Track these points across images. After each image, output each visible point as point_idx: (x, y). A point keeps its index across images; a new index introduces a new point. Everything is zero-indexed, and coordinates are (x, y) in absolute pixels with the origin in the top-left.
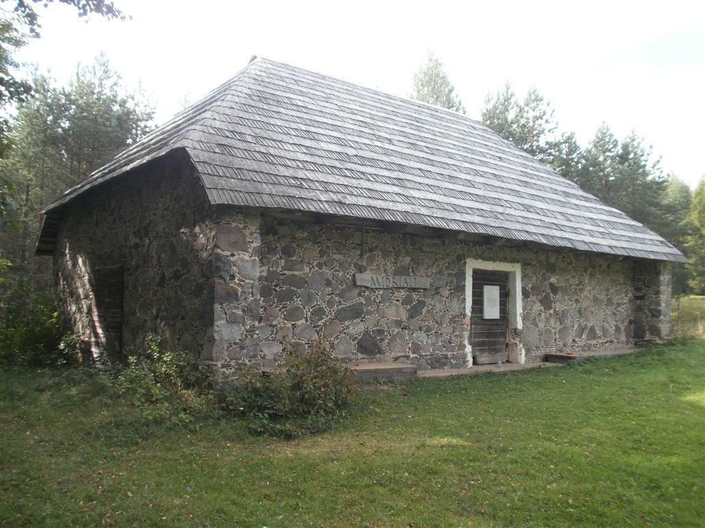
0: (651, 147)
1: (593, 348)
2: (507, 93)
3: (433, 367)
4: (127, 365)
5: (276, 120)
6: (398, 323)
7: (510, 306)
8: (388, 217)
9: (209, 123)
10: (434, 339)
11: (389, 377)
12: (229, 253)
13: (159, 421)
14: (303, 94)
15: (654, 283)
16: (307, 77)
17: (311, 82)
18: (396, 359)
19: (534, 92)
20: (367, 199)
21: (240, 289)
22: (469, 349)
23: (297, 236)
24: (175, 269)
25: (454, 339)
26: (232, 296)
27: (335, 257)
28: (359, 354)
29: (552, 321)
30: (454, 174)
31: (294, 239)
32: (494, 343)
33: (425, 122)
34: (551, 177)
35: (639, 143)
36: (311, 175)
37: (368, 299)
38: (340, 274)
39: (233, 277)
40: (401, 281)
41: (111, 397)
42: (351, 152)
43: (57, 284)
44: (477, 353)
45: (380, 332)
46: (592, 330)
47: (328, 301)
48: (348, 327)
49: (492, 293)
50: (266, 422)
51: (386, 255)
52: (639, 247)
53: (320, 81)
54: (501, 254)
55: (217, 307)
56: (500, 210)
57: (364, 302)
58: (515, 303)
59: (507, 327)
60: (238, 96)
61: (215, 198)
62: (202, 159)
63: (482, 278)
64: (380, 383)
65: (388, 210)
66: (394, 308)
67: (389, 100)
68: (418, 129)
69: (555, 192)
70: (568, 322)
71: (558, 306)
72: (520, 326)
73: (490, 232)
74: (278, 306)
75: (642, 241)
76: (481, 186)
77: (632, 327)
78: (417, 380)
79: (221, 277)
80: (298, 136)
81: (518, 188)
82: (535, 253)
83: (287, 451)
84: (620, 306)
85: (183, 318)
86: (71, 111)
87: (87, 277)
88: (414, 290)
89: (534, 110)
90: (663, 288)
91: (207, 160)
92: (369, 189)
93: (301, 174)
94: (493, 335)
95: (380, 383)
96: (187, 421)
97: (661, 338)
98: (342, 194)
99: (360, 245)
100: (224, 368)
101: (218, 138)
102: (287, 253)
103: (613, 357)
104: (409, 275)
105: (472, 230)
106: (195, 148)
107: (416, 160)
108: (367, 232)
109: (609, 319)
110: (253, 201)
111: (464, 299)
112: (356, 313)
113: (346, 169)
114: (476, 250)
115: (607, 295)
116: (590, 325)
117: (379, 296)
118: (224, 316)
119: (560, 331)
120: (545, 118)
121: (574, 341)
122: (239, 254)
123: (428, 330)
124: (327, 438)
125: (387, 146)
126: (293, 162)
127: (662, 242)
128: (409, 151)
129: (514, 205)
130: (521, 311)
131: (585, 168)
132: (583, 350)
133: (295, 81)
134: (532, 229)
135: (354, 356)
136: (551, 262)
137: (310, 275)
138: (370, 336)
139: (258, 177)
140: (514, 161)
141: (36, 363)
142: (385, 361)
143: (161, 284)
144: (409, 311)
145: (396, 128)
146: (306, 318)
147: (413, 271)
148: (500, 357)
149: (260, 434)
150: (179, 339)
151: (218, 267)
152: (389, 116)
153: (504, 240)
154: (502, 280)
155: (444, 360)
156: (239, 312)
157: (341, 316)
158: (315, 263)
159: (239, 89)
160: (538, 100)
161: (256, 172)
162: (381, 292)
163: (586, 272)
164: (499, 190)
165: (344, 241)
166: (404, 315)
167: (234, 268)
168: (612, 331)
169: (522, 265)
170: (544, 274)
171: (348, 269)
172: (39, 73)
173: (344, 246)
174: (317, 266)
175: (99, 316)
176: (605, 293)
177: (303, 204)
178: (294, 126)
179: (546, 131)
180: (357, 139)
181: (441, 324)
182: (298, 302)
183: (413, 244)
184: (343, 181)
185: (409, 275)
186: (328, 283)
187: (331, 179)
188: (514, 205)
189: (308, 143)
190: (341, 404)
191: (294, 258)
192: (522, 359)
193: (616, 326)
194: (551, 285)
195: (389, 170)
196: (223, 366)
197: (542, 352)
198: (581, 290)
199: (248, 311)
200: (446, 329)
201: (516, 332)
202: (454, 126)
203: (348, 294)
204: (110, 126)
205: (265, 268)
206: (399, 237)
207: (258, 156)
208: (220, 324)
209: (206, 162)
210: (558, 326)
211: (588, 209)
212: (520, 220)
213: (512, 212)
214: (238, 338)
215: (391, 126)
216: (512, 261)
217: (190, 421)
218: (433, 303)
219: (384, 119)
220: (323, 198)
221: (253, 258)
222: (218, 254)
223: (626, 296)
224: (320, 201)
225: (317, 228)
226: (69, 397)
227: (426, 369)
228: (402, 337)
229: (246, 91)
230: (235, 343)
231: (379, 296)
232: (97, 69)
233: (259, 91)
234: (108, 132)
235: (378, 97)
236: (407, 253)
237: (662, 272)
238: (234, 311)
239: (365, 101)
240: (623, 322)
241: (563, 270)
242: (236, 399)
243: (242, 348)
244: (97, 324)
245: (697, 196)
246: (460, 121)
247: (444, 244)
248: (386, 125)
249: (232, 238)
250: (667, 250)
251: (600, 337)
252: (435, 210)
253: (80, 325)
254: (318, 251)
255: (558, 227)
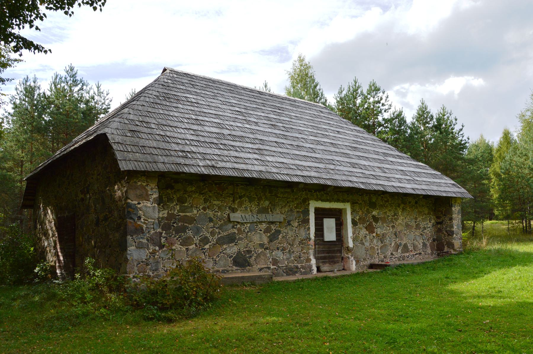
0: (456, 120)
1: (406, 259)
2: (355, 86)
3: (288, 275)
4: (74, 279)
5: (175, 113)
6: (262, 245)
7: (344, 232)
8: (246, 175)
9: (125, 116)
10: (288, 255)
11: (252, 281)
12: (136, 202)
13: (85, 315)
14: (197, 94)
15: (449, 212)
16: (201, 82)
17: (205, 86)
18: (261, 270)
19: (373, 85)
20: (233, 164)
21: (145, 226)
22: (313, 262)
23: (188, 189)
24: (105, 214)
25: (302, 255)
26: (139, 230)
27: (215, 202)
28: (234, 267)
29: (375, 241)
30: (301, 144)
31: (186, 192)
32: (333, 257)
33: (285, 110)
34: (375, 143)
35: (448, 117)
36: (194, 149)
37: (239, 230)
38: (219, 214)
39: (139, 218)
40: (262, 217)
41: (59, 301)
42: (226, 132)
43: (36, 227)
44: (321, 264)
45: (249, 252)
46: (405, 246)
47: (211, 232)
48: (225, 249)
49: (329, 224)
50: (155, 312)
51: (251, 200)
52: (435, 188)
53: (210, 84)
54: (336, 197)
55: (129, 238)
56: (332, 167)
57: (237, 232)
58: (347, 230)
59: (342, 246)
60: (149, 97)
61: (124, 166)
62: (117, 141)
63: (321, 214)
64: (246, 286)
65: (248, 170)
66: (258, 235)
67: (260, 96)
68: (279, 114)
69: (377, 153)
70: (387, 242)
71: (379, 231)
72: (351, 244)
73: (322, 182)
74: (175, 236)
75: (439, 185)
76: (320, 152)
77: (435, 243)
78: (273, 283)
79: (132, 218)
80: (189, 123)
81: (349, 152)
82: (360, 195)
83: (165, 329)
84: (425, 229)
85: (110, 247)
86: (51, 109)
87: (53, 223)
88: (272, 223)
89: (374, 97)
90: (454, 216)
91: (120, 141)
92: (236, 157)
93: (187, 149)
94: (331, 252)
95: (246, 286)
96: (105, 313)
97: (455, 250)
98: (215, 161)
99: (232, 194)
100: (134, 277)
101: (130, 126)
102: (181, 201)
103: (419, 264)
104: (268, 213)
105: (309, 181)
106: (112, 134)
107: (274, 135)
108: (237, 185)
109: (418, 239)
110: (150, 167)
111: (309, 228)
112: (231, 239)
113: (221, 144)
114: (317, 195)
115: (416, 222)
116: (403, 243)
117: (247, 228)
118: (134, 243)
119: (381, 248)
120: (382, 102)
121: (392, 254)
122: (143, 203)
123: (284, 249)
124: (195, 321)
125: (254, 127)
126: (183, 141)
127: (453, 184)
128: (270, 130)
129: (343, 163)
130: (352, 235)
131: (411, 135)
132: (399, 260)
133: (192, 85)
134: (355, 179)
135: (230, 269)
136: (372, 201)
137: (198, 215)
138: (242, 255)
139: (155, 152)
140: (351, 132)
141: (19, 282)
142: (253, 271)
143: (97, 224)
144: (269, 237)
145: (263, 114)
146: (196, 244)
147: (271, 211)
148: (336, 267)
149: (151, 319)
150: (108, 261)
151: (128, 212)
152: (258, 107)
153: (333, 187)
154: (338, 215)
155: (295, 270)
156: (145, 241)
157: (221, 241)
158: (201, 207)
159: (150, 92)
160: (377, 90)
161: (155, 148)
162: (249, 225)
163: (399, 207)
164: (334, 154)
165: (221, 192)
166: (265, 240)
167: (140, 212)
168: (420, 246)
169: (351, 204)
170: (368, 209)
171: (225, 210)
172: (28, 84)
173: (222, 195)
174: (202, 209)
175: (61, 248)
176: (414, 220)
177: (186, 168)
178: (187, 116)
179: (383, 111)
180: (232, 123)
181: (292, 245)
182: (190, 233)
183: (270, 192)
184: (217, 152)
185: (268, 213)
186: (211, 220)
187: (209, 151)
188: (343, 163)
189: (195, 127)
190: (209, 299)
191: (186, 205)
192: (353, 267)
193: (424, 243)
194: (374, 217)
195: (253, 143)
196: (134, 277)
197: (368, 262)
198: (396, 219)
199: (151, 240)
200: (297, 248)
201: (348, 250)
202: (307, 111)
203: (224, 227)
204: (77, 119)
205: (166, 212)
206: (260, 188)
207: (158, 138)
208: (131, 249)
209: (119, 143)
210: (380, 244)
211: (401, 164)
212: (346, 173)
213: (341, 168)
214: (144, 258)
215: (259, 114)
216: (344, 201)
217: (107, 314)
218: (286, 231)
219: (254, 109)
220: (201, 164)
221: (154, 205)
222: (129, 203)
223: (430, 222)
224: (199, 166)
225: (202, 184)
226: (33, 302)
227: (283, 276)
228: (265, 255)
229: (155, 93)
230: (142, 262)
231: (247, 228)
232: (68, 78)
233: (165, 93)
234: (77, 122)
235: (252, 94)
236: (267, 199)
237: (453, 205)
238: (141, 240)
239: (242, 97)
240: (428, 240)
241: (382, 206)
242: (139, 298)
243: (147, 265)
244: (60, 254)
245: (497, 152)
246: (312, 107)
247: (293, 191)
248: (256, 113)
249: (138, 192)
250: (457, 190)
251: (411, 251)
252: (282, 169)
253: (49, 255)
254: (203, 199)
255: (375, 177)
